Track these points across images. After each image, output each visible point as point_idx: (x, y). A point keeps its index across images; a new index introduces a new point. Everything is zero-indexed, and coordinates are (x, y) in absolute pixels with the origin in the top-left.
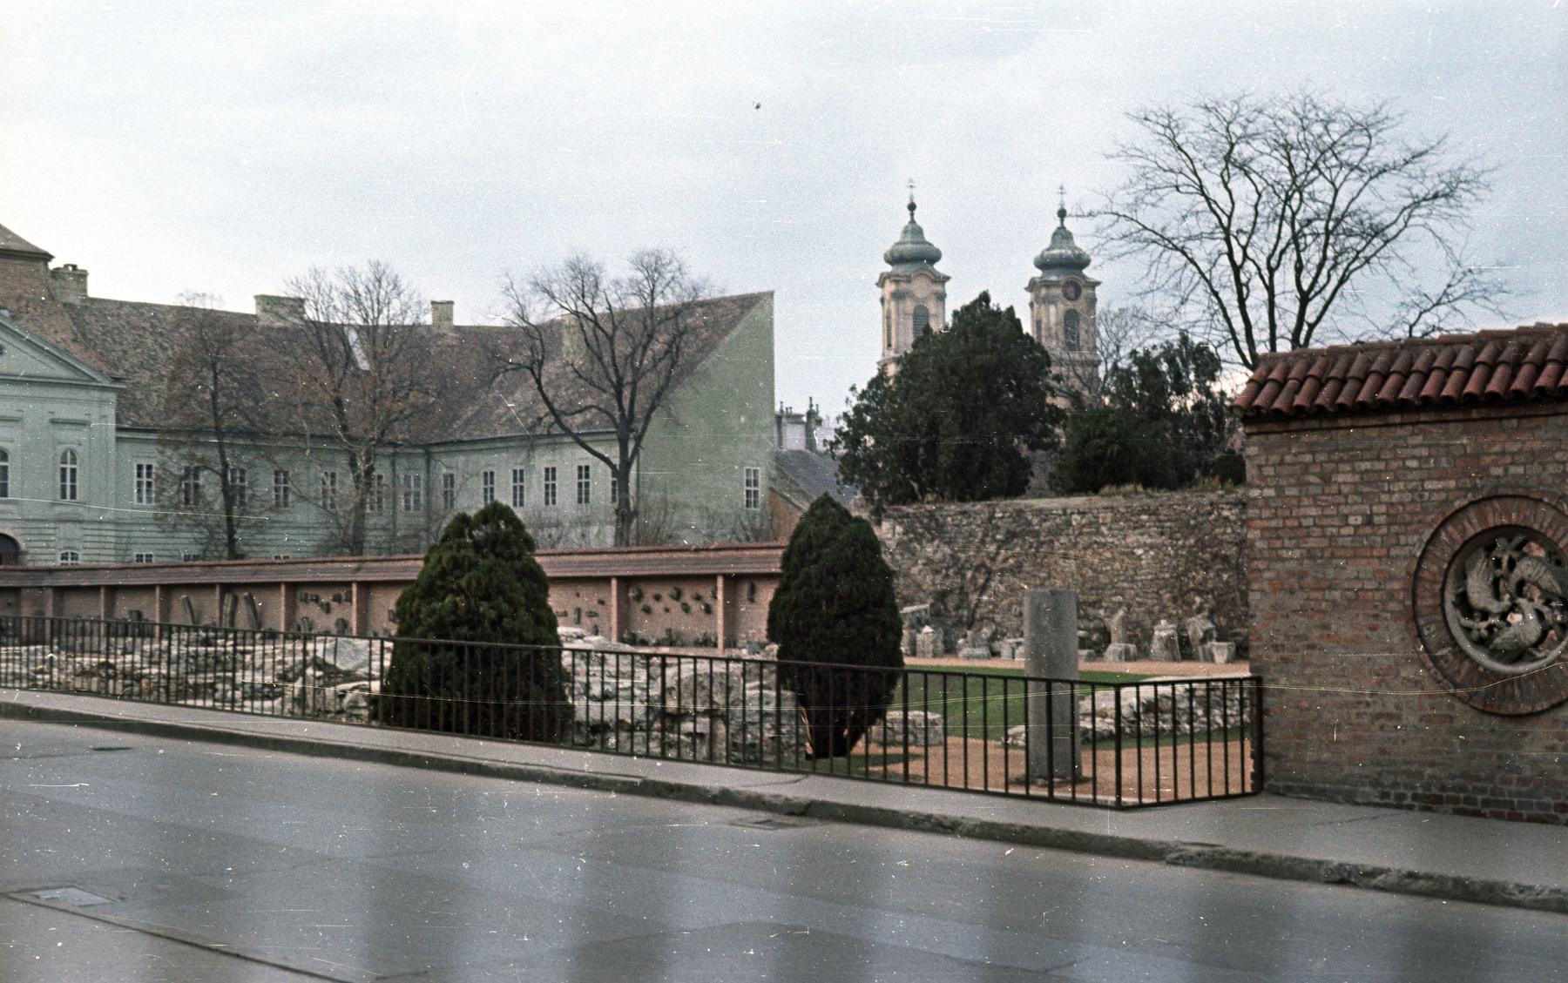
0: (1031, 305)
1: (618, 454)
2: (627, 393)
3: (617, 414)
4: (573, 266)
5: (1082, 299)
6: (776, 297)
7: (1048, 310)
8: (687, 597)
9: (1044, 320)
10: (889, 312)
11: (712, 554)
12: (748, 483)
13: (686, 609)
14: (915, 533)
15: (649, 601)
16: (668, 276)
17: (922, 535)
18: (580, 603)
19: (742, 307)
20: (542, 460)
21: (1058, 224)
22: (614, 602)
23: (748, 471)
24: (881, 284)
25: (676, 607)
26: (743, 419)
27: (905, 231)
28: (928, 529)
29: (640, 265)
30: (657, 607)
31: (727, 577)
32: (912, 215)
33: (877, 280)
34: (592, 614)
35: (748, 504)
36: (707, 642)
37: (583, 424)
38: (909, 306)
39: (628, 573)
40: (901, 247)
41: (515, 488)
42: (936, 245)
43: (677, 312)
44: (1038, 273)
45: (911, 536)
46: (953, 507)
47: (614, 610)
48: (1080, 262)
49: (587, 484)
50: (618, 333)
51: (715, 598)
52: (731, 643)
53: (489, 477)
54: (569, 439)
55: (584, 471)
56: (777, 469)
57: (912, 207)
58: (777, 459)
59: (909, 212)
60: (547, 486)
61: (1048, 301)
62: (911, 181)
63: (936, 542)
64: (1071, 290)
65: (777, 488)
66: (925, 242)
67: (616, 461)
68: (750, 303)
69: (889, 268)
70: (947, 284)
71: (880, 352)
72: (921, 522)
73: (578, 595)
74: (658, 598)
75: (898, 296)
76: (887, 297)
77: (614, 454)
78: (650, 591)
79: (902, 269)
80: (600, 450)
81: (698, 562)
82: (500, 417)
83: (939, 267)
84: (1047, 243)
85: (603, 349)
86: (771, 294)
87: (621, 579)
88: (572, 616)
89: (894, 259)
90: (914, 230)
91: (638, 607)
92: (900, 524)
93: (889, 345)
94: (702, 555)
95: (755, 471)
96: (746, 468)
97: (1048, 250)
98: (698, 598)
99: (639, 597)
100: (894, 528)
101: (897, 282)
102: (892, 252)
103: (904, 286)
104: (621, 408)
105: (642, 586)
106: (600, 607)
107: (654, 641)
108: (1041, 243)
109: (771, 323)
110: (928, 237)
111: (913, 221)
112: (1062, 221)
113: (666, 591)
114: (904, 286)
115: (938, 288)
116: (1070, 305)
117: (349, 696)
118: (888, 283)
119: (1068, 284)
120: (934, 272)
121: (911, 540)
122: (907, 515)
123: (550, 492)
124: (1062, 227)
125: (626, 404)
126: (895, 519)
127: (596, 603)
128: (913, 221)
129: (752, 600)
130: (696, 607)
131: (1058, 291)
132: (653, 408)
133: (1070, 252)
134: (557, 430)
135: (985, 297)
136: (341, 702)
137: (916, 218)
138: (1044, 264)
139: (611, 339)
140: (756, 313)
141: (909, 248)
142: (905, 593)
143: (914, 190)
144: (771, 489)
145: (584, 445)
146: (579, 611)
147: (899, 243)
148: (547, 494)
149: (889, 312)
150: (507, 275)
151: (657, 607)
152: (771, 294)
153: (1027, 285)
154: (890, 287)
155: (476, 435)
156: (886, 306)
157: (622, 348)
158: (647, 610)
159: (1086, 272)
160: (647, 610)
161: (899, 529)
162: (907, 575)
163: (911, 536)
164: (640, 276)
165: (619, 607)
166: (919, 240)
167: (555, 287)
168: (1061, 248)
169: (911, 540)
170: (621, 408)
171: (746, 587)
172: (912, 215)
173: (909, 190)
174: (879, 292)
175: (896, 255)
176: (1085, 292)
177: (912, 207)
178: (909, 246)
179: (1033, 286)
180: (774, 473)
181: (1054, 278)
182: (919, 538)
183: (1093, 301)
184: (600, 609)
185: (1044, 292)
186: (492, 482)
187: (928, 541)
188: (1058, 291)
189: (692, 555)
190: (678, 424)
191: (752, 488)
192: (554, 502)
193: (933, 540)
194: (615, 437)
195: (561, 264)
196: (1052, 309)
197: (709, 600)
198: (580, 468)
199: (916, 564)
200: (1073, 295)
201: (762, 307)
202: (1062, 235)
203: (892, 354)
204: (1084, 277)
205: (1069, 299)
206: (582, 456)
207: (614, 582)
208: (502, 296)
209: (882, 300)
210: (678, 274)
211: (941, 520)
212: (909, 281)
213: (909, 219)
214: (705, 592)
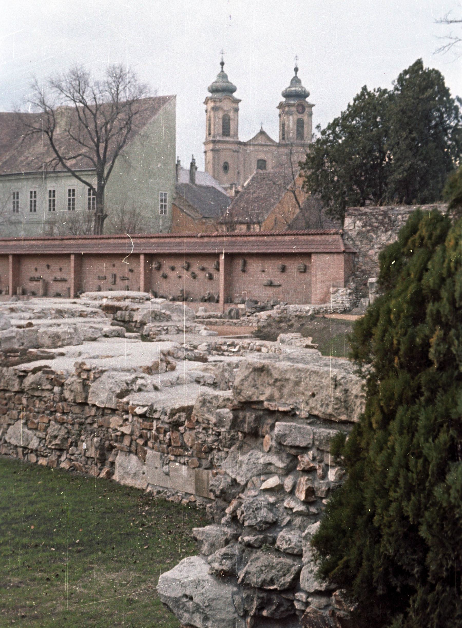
0: (280, 116)
1: (96, 183)
2: (102, 146)
3: (96, 159)
4: (73, 73)
5: (306, 112)
6: (177, 98)
7: (288, 118)
8: (195, 268)
9: (287, 123)
10: (210, 117)
11: (213, 240)
12: (162, 201)
13: (194, 276)
14: (371, 225)
15: (166, 269)
16: (127, 81)
17: (377, 228)
18: (114, 270)
19: (159, 103)
20: (50, 185)
21: (294, 75)
22: (142, 269)
23: (162, 194)
24: (206, 103)
25: (186, 275)
26: (159, 165)
27: (219, 76)
28: (382, 223)
29: (110, 74)
30: (173, 275)
31: (226, 254)
32: (222, 68)
33: (204, 101)
34: (124, 279)
35: (161, 213)
36: (210, 299)
37: (76, 164)
38: (220, 114)
39: (150, 252)
40: (218, 84)
41: (31, 201)
42: (234, 84)
43: (130, 103)
44: (284, 99)
45: (369, 228)
46: (402, 208)
47: (142, 276)
48: (305, 95)
49: (74, 200)
50: (98, 112)
51: (218, 270)
52: (229, 300)
53: (16, 195)
54: (69, 174)
55: (72, 192)
56: (177, 193)
57: (222, 64)
58: (176, 188)
59: (220, 66)
60: (50, 201)
61: (288, 114)
62: (222, 50)
63: (390, 233)
64: (300, 108)
65: (177, 204)
66: (228, 82)
67: (95, 187)
68: (163, 101)
69: (210, 95)
70: (240, 104)
71: (205, 137)
72: (377, 219)
73: (114, 265)
74: (173, 269)
75: (215, 109)
76: (209, 109)
77: (94, 182)
78: (167, 264)
79: (216, 95)
80: (84, 179)
81: (202, 244)
82: (22, 162)
83: (235, 95)
84: (288, 84)
85: (89, 120)
86: (175, 97)
87: (146, 255)
88: (110, 279)
89: (213, 90)
90: (223, 76)
91: (158, 276)
92: (360, 220)
93: (210, 134)
94: (206, 240)
95: (165, 194)
96: (160, 192)
97: (289, 87)
98: (203, 269)
99: (159, 268)
100: (355, 223)
101: (215, 101)
102: (212, 86)
103: (218, 104)
104: (98, 155)
105: (161, 260)
106: (130, 273)
107: (171, 298)
108: (285, 84)
109: (175, 113)
110: (230, 79)
111: (222, 71)
112: (296, 73)
113: (180, 264)
114: (218, 104)
115: (234, 105)
116: (300, 116)
117: (31, 378)
118: (209, 101)
119: (298, 106)
120: (233, 97)
121: (368, 231)
122: (365, 214)
123: (52, 204)
124: (296, 77)
125: (101, 151)
126: (355, 216)
127: (127, 271)
128: (222, 71)
129: (244, 271)
130: (201, 275)
131: (294, 109)
132: (116, 156)
133: (300, 89)
134: (59, 168)
135: (419, 63)
136: (21, 382)
137: (224, 69)
138: (287, 95)
139: (95, 115)
140: (167, 106)
141: (221, 84)
142: (363, 268)
143: (224, 56)
144: (173, 204)
145: (77, 177)
146: (115, 276)
147: (216, 82)
148: (50, 205)
149: (210, 117)
150: (34, 77)
151: (173, 275)
152: (175, 97)
153: (278, 105)
154: (211, 104)
155: (9, 172)
156: (208, 114)
157: (101, 121)
158: (165, 277)
159: (308, 99)
160: (165, 277)
161: (359, 223)
162: (365, 256)
163: (369, 228)
164: (110, 80)
165: (145, 274)
166: (225, 80)
167: (63, 84)
168: (296, 87)
169: (368, 231)
170: (98, 155)
171: (241, 262)
172: (222, 68)
173: (221, 55)
174: (204, 107)
175: (214, 88)
176: (307, 109)
177: (222, 64)
178: (221, 84)
179: (281, 106)
180: (175, 195)
181: (292, 102)
182: (375, 230)
183: (310, 114)
184: (130, 276)
185: (287, 109)
186: (18, 198)
187: (382, 232)
188: (294, 109)
189: (198, 240)
190: (130, 165)
191: (164, 204)
192: (54, 210)
193: (386, 231)
194: (95, 173)
195: (67, 71)
196: (291, 118)
197: (213, 272)
198: (69, 191)
199: (372, 248)
200: (301, 111)
201: (170, 103)
202: (296, 81)
203: (211, 138)
204: (307, 102)
205: (299, 113)
206: (73, 183)
207: (142, 257)
208: (31, 90)
209: (206, 111)
210: (132, 80)
211: (393, 218)
212: (220, 101)
213: (220, 69)
214: (210, 265)
